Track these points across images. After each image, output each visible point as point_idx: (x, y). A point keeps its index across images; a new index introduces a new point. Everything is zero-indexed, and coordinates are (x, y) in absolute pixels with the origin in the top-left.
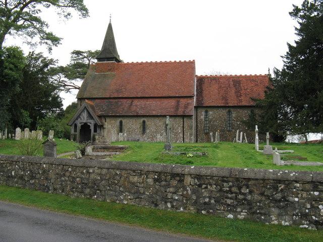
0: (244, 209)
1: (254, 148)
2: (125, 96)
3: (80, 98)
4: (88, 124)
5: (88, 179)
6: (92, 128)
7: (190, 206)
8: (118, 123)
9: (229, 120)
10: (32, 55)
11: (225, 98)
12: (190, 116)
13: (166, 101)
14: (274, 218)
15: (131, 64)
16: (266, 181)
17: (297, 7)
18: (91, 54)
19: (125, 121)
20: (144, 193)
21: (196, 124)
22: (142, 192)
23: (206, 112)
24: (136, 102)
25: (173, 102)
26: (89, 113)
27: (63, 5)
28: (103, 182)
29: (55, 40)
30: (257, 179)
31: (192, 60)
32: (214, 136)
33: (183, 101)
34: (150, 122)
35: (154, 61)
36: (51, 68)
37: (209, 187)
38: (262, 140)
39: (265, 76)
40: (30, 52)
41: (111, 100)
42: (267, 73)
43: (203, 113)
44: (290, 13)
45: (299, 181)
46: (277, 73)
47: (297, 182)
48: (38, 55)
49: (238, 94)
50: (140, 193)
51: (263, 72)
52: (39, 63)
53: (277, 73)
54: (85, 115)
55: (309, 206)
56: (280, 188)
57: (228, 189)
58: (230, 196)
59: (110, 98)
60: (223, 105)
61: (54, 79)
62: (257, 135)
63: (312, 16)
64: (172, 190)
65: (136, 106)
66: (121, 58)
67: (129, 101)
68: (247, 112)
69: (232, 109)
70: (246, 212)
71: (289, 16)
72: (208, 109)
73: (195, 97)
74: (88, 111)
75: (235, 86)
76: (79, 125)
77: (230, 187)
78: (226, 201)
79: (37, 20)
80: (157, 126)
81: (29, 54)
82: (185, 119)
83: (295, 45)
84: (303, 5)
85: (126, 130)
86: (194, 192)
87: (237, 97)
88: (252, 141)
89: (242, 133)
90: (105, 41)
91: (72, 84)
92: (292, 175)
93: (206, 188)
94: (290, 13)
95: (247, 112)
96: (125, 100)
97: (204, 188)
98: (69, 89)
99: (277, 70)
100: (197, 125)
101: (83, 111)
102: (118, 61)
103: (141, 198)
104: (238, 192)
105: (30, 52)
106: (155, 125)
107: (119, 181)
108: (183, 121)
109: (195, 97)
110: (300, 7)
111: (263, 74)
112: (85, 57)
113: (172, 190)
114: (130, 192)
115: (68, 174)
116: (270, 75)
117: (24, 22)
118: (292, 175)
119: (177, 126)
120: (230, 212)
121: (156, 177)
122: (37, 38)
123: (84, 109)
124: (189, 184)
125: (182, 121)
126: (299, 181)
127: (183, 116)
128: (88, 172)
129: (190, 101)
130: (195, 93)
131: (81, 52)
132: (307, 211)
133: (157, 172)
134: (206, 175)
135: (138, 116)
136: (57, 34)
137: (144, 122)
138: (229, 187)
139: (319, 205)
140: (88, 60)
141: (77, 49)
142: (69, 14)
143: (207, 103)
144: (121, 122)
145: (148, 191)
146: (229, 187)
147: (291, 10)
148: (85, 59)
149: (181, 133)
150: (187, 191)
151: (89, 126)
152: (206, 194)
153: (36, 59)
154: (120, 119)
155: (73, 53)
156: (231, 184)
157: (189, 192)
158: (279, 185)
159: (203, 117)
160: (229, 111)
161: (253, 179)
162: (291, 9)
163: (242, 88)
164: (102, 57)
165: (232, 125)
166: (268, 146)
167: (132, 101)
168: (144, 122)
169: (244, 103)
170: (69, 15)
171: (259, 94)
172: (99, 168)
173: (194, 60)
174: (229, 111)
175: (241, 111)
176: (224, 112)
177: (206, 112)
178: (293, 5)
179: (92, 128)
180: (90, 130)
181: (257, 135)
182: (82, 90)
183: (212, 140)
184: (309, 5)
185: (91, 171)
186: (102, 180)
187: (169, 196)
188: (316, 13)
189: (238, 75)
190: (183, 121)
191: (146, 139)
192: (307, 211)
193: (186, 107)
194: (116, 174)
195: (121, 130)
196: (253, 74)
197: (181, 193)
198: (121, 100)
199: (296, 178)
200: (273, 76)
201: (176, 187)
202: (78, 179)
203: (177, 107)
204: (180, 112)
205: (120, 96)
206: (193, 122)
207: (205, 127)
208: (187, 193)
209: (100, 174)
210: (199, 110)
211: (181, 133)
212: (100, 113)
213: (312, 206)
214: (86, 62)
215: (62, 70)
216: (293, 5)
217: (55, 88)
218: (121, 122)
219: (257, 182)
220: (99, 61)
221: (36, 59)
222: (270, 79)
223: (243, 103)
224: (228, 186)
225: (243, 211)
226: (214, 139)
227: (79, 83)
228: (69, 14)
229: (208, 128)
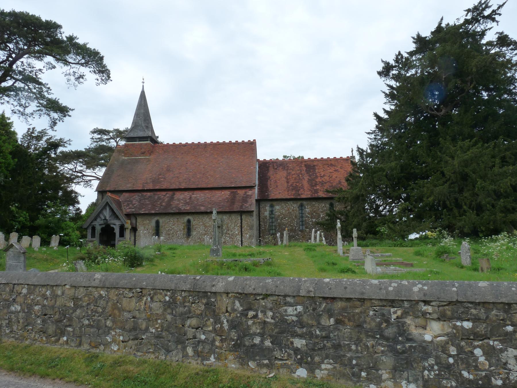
0: (327, 357)
1: (336, 251)
2: (164, 187)
3: (101, 192)
4: (112, 226)
5: (53, 307)
6: (117, 231)
7: (227, 352)
8: (153, 223)
9: (302, 217)
10: (32, 133)
11: (296, 189)
12: (250, 212)
13: (218, 193)
14: (385, 376)
15: (171, 145)
16: (367, 304)
17: (388, 63)
18: (119, 134)
19: (162, 220)
20: (147, 329)
21: (258, 223)
22: (144, 326)
23: (272, 206)
24: (179, 196)
25: (227, 193)
26: (112, 210)
27: (73, 62)
28: (78, 311)
29: (63, 111)
30: (349, 300)
31: (252, 140)
32: (282, 237)
33: (241, 192)
34: (195, 221)
35: (202, 142)
36: (62, 152)
37: (260, 315)
38: (347, 237)
39: (348, 159)
40: (29, 129)
41: (145, 194)
42: (350, 155)
43: (268, 208)
44: (380, 73)
45: (431, 301)
46: (361, 152)
47: (427, 303)
48: (39, 132)
49: (313, 183)
50: (141, 329)
51: (346, 154)
52: (42, 143)
53: (361, 152)
54: (107, 213)
55: (453, 351)
56: (394, 316)
57: (295, 319)
58: (299, 331)
59: (143, 191)
60: (293, 197)
61: (66, 168)
62: (339, 233)
63: (408, 75)
64: (194, 322)
65: (179, 200)
66: (160, 140)
67: (170, 194)
68: (324, 206)
69: (305, 203)
70: (331, 364)
71: (378, 76)
72: (274, 203)
73: (256, 188)
74: (112, 210)
75: (308, 172)
76: (98, 229)
77: (299, 315)
78: (292, 343)
79: (36, 81)
80: (206, 227)
81: (28, 131)
82: (244, 217)
83: (415, 49)
84: (397, 61)
85: (164, 232)
86: (233, 325)
87: (312, 186)
88: (332, 242)
89: (319, 232)
90: (137, 115)
91: (94, 175)
92: (416, 289)
93: (255, 317)
94: (380, 73)
95: (324, 206)
96: (164, 193)
97: (251, 318)
98: (90, 180)
99: (362, 150)
100: (260, 224)
101: (104, 208)
102: (154, 140)
103: (143, 339)
104: (315, 323)
105: (29, 129)
106: (204, 224)
107: (104, 308)
108: (241, 219)
109: (256, 188)
110: (392, 63)
111: (345, 156)
112: (111, 138)
113: (194, 322)
114: (123, 329)
115: (20, 299)
116: (353, 157)
117: (14, 83)
118: (416, 289)
119: (233, 225)
120: (300, 363)
121: (167, 298)
122: (33, 106)
123: (106, 205)
124: (224, 310)
125: (239, 218)
126: (431, 301)
127: (241, 213)
128: (55, 296)
129: (250, 192)
130: (257, 183)
131: (105, 131)
132: (451, 360)
133: (168, 290)
134: (254, 292)
135: (181, 213)
136: (63, 102)
137: (189, 221)
138: (296, 316)
139: (475, 347)
140: (116, 141)
141: (100, 127)
142: (81, 77)
143: (274, 194)
144: (157, 223)
145: (153, 326)
146: (296, 316)
147: (380, 69)
148: (112, 140)
149: (238, 234)
150: (222, 323)
151: (498, 235)
152: (256, 329)
153: (39, 138)
154: (156, 219)
155: (94, 132)
156: (300, 308)
157: (226, 325)
158: (392, 310)
159: (267, 214)
160: (302, 205)
161: (341, 299)
162: (380, 67)
163: (318, 174)
164: (132, 135)
165: (303, 223)
166: (355, 248)
167: (174, 194)
168: (189, 221)
169: (321, 194)
170: (83, 78)
171: (340, 182)
172: (72, 286)
173: (255, 140)
174: (302, 205)
175: (316, 204)
176: (294, 206)
177: (272, 206)
178: (383, 61)
179: (117, 231)
180: (115, 234)
181: (339, 233)
182: (103, 181)
183: (280, 243)
184: (404, 60)
185: (59, 293)
186: (77, 306)
187: (190, 333)
188: (413, 71)
189: (312, 158)
190: (241, 219)
191: (192, 244)
192: (451, 360)
193: (245, 200)
194: (101, 296)
195: (157, 233)
196: (332, 157)
197: (211, 328)
198: (289, 197)
199: (425, 295)
200: (357, 158)
201: (199, 316)
202: (37, 308)
203: (232, 200)
204: (236, 208)
205: (157, 188)
206: (254, 220)
207: (270, 226)
208: (222, 327)
209: (75, 299)
210: (262, 205)
211: (238, 234)
212: (128, 210)
213: (460, 350)
214: (113, 143)
215: (76, 156)
216: (383, 61)
217: (70, 180)
218: (157, 223)
219: (348, 304)
220: (128, 141)
221: (39, 138)
222: (353, 164)
223: (319, 194)
224: (295, 312)
225: (326, 361)
226: (282, 241)
227: (101, 172)
228: (81, 77)
229: (274, 228)
